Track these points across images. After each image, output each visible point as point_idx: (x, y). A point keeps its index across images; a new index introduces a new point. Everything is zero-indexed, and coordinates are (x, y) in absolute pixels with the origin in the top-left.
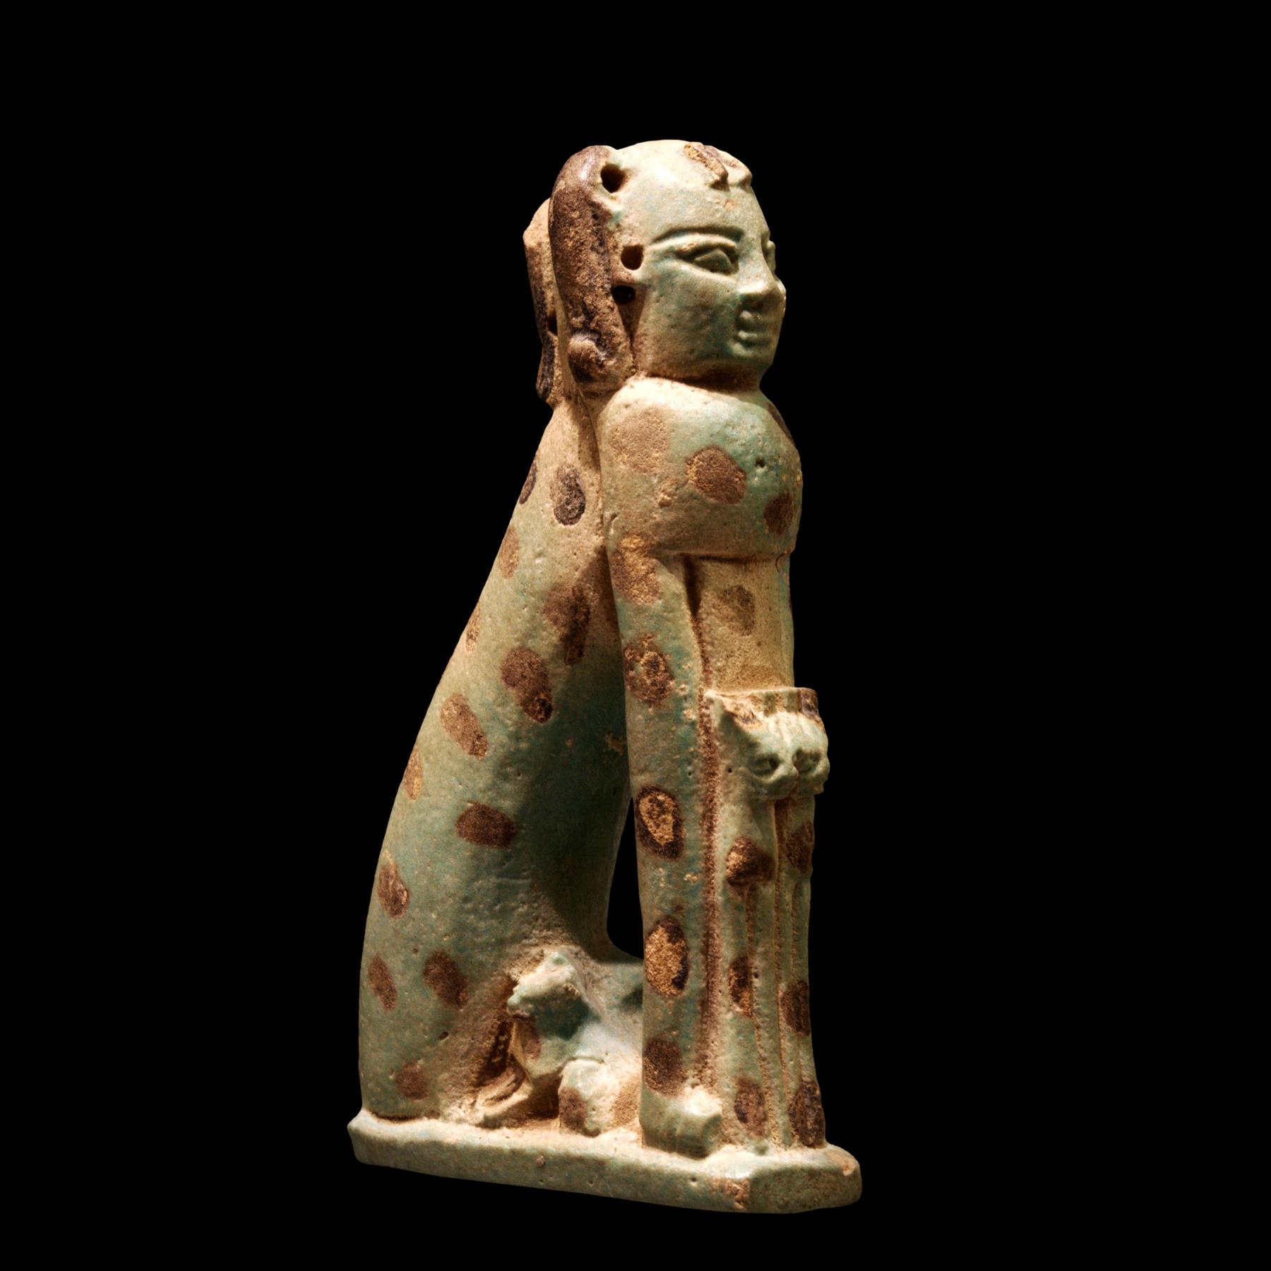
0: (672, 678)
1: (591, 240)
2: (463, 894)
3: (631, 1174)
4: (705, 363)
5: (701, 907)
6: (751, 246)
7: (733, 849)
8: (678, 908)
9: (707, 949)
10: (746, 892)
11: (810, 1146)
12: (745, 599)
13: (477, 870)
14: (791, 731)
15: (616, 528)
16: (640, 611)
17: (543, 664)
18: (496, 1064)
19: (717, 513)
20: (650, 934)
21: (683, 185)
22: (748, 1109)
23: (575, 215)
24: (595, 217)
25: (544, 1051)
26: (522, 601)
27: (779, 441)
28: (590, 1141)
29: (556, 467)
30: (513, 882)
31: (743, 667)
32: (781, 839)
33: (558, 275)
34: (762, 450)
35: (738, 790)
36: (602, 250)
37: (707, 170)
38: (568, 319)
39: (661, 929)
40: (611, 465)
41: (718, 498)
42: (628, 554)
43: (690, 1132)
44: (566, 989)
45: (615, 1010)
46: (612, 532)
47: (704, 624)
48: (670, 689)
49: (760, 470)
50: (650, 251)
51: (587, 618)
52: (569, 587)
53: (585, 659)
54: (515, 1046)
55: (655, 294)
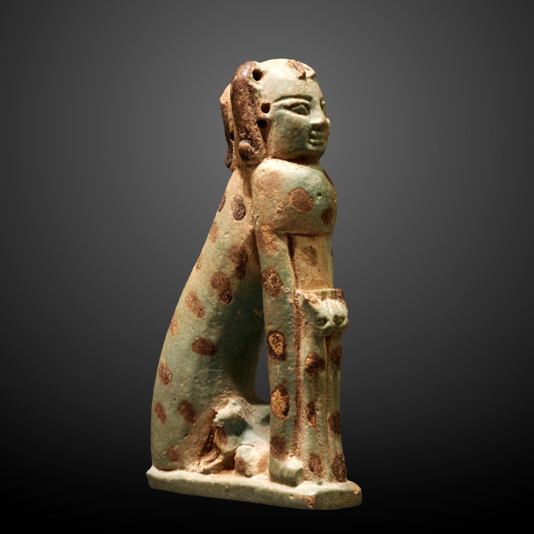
0: (282, 285)
1: (249, 101)
2: (194, 375)
3: (265, 493)
4: (296, 152)
5: (295, 381)
6: (316, 103)
7: (308, 357)
8: (285, 382)
9: (297, 399)
10: (313, 375)
11: (340, 481)
12: (313, 252)
13: (200, 366)
14: (331, 308)
15: (259, 222)
16: (269, 257)
17: (228, 279)
18: (208, 447)
19: (301, 215)
20: (273, 392)
21: (287, 78)
22: (314, 466)
23: (242, 90)
24: (250, 91)
25: (228, 442)
26: (219, 252)
27: (327, 185)
28: (248, 480)
29: (233, 196)
30: (215, 370)
31: (312, 280)
32: (328, 352)
33: (235, 116)
34: (320, 189)
35: (310, 332)
36: (253, 105)
37: (297, 72)
38: (239, 134)
39: (278, 390)
40: (257, 195)
41: (302, 209)
42: (264, 233)
43: (290, 476)
44: (238, 415)
45: (259, 424)
46: (257, 223)
47: (296, 262)
48: (281, 290)
49: (319, 198)
50: (273, 105)
51: (247, 261)
52: (239, 247)
53: (246, 277)
54: (216, 440)
55: (275, 124)
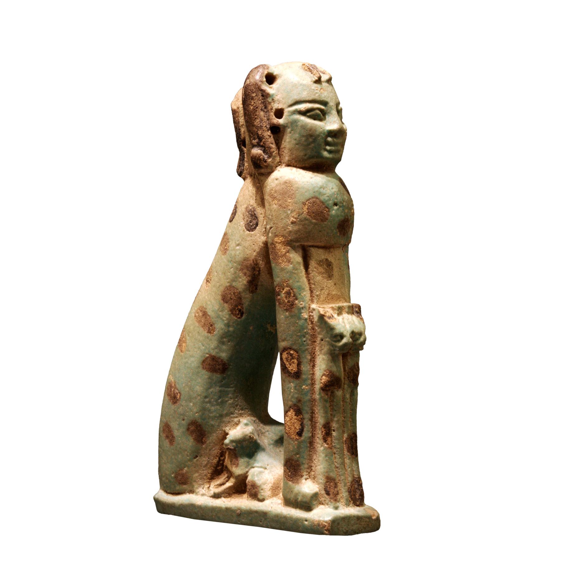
0: (297, 299)
1: (261, 106)
2: (204, 394)
4: (311, 160)
5: (309, 400)
6: (332, 109)
7: (324, 375)
8: (299, 401)
9: (312, 419)
10: (329, 394)
12: (329, 264)
13: (210, 384)
15: (272, 233)
16: (282, 270)
17: (240, 293)
18: (219, 470)
19: (316, 226)
21: (301, 82)
23: (254, 95)
24: (263, 96)
25: (240, 464)
26: (230, 265)
27: (344, 195)
28: (260, 504)
29: (245, 206)
30: (226, 389)
31: (328, 294)
32: (345, 370)
33: (247, 121)
34: (336, 198)
35: (326, 349)
36: (266, 110)
37: (312, 75)
38: (251, 141)
39: (292, 410)
40: (270, 205)
41: (317, 220)
42: (277, 245)
43: (304, 500)
44: (250, 436)
46: (270, 235)
47: (311, 275)
48: (296, 304)
49: (335, 208)
50: (287, 111)
52: (251, 259)
53: (258, 291)
54: (227, 462)
55: (289, 130)
